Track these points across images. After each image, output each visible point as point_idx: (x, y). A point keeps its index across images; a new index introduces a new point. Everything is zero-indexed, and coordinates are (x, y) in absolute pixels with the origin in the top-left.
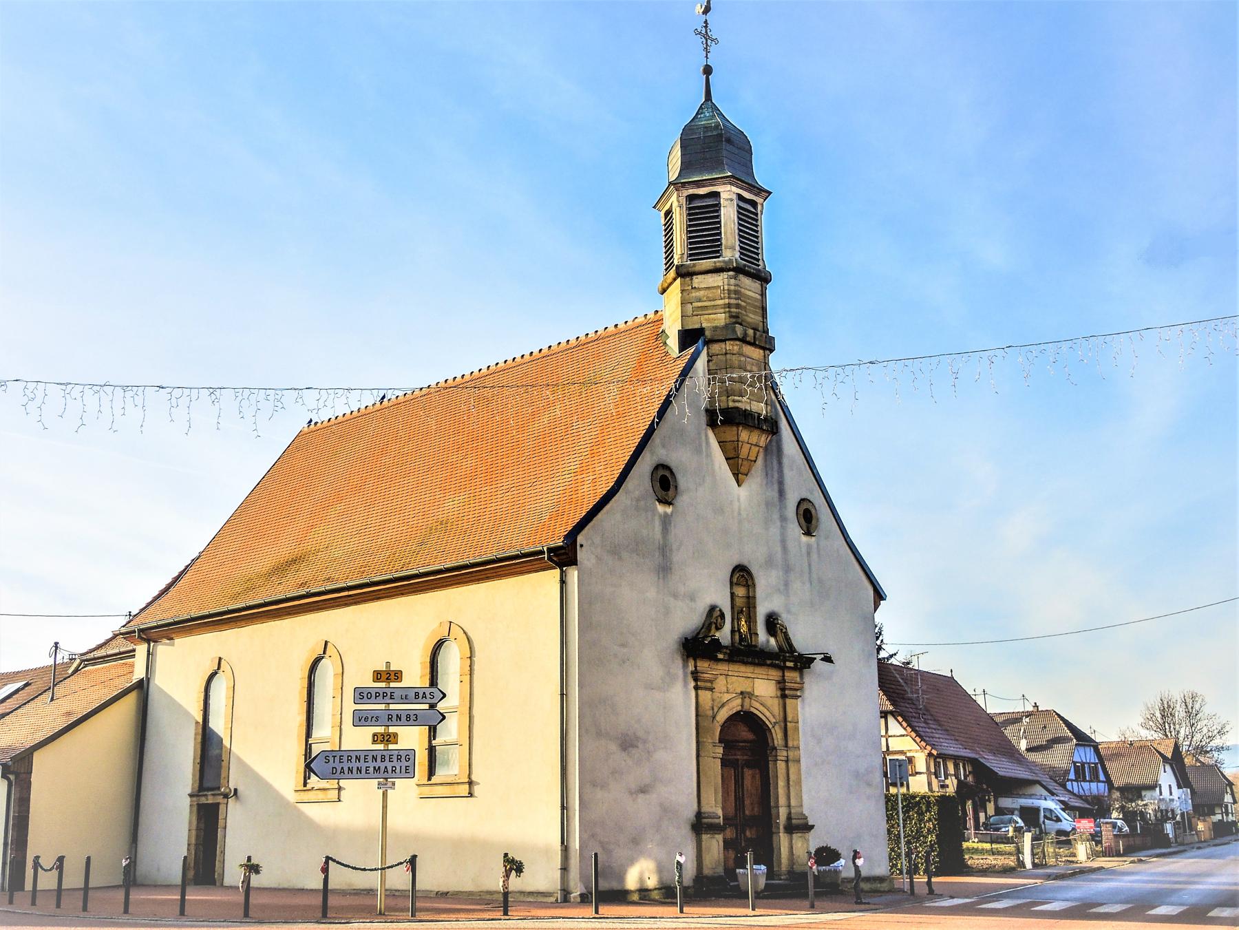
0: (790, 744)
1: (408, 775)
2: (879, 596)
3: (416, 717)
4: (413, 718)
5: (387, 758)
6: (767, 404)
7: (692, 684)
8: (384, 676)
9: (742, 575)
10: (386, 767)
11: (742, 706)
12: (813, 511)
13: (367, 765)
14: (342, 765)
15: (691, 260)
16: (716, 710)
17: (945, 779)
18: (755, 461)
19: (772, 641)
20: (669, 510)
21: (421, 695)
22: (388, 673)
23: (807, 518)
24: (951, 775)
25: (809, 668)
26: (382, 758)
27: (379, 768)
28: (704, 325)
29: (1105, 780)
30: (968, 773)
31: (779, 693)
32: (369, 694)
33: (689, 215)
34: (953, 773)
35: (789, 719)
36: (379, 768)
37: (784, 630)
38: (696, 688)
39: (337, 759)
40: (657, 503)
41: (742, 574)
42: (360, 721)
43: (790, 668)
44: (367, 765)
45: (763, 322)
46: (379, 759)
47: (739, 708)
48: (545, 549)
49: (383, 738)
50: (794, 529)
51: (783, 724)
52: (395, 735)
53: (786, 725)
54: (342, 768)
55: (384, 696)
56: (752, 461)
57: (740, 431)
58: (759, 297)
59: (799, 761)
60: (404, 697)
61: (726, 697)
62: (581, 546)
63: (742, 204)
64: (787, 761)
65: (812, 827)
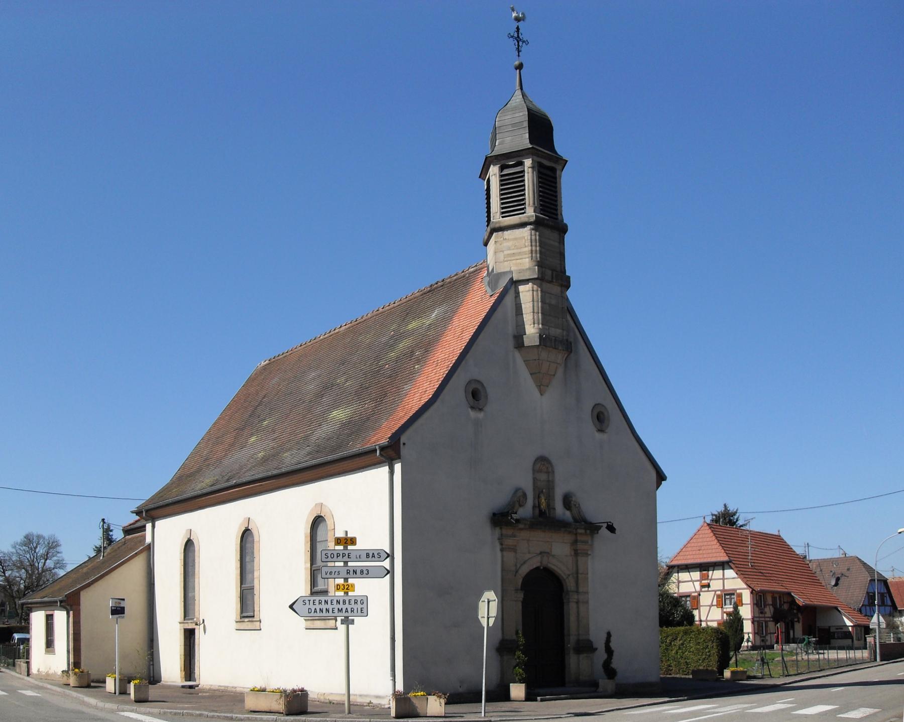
0: (581, 590)
1: (362, 614)
2: (661, 477)
3: (368, 572)
4: (365, 572)
5: (347, 602)
6: (563, 330)
7: (498, 547)
8: (343, 541)
9: (543, 464)
10: (347, 609)
11: (541, 563)
12: (606, 414)
13: (333, 606)
14: (315, 607)
15: (503, 217)
16: (518, 566)
17: (764, 607)
18: (554, 375)
19: (568, 513)
20: (481, 415)
21: (371, 555)
22: (346, 539)
23: (600, 418)
24: (769, 605)
25: (598, 533)
26: (343, 602)
27: (342, 609)
28: (513, 269)
29: (891, 604)
30: (782, 603)
31: (573, 553)
32: (332, 557)
33: (501, 181)
34: (771, 603)
35: (580, 571)
36: (342, 609)
37: (577, 506)
38: (502, 550)
39: (312, 602)
40: (470, 409)
41: (543, 463)
42: (326, 574)
43: (581, 534)
44: (333, 606)
45: (561, 264)
46: (341, 602)
47: (538, 565)
48: (377, 447)
49: (344, 587)
50: (589, 426)
51: (575, 576)
52: (353, 585)
53: (577, 577)
54: (315, 609)
55: (343, 556)
56: (551, 375)
57: (539, 352)
58: (557, 244)
59: (587, 602)
60: (358, 557)
61: (528, 556)
62: (404, 444)
63: (542, 170)
64: (577, 603)
65: (597, 649)
